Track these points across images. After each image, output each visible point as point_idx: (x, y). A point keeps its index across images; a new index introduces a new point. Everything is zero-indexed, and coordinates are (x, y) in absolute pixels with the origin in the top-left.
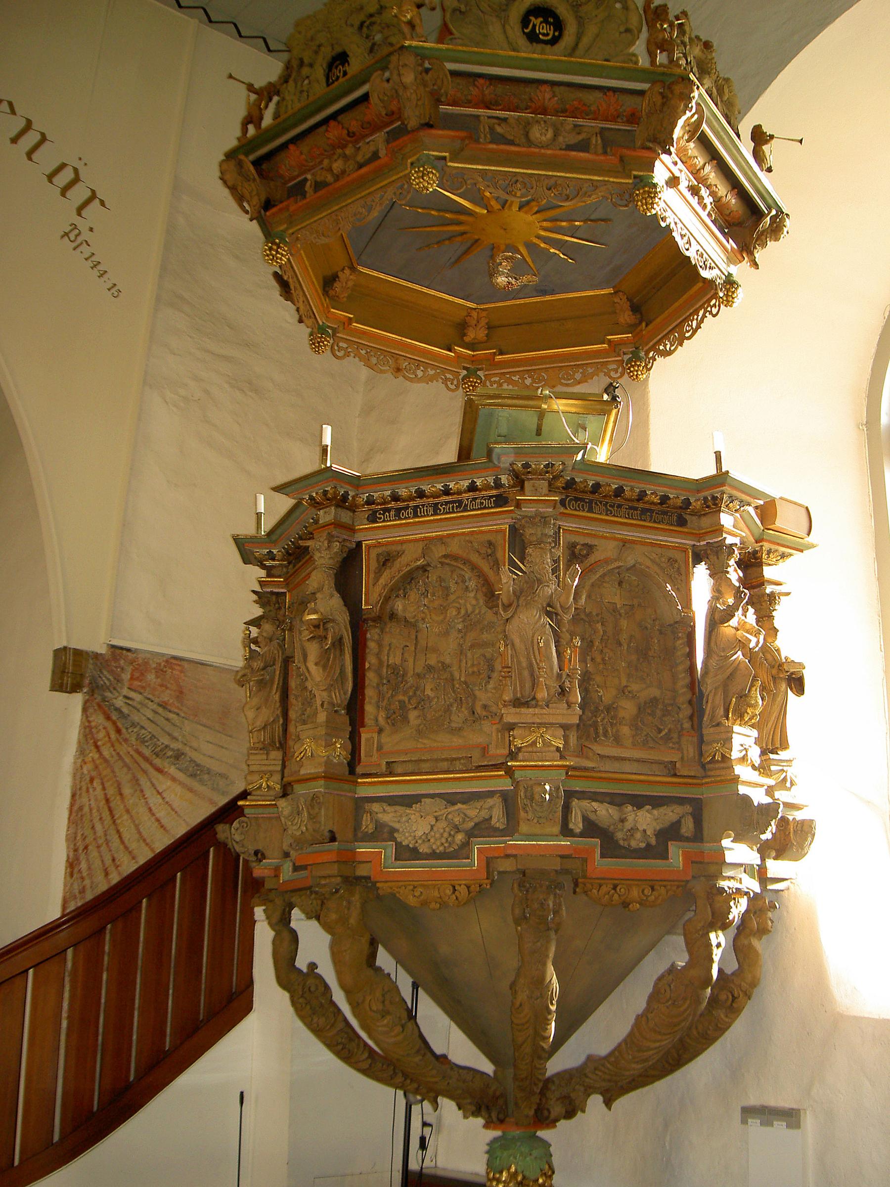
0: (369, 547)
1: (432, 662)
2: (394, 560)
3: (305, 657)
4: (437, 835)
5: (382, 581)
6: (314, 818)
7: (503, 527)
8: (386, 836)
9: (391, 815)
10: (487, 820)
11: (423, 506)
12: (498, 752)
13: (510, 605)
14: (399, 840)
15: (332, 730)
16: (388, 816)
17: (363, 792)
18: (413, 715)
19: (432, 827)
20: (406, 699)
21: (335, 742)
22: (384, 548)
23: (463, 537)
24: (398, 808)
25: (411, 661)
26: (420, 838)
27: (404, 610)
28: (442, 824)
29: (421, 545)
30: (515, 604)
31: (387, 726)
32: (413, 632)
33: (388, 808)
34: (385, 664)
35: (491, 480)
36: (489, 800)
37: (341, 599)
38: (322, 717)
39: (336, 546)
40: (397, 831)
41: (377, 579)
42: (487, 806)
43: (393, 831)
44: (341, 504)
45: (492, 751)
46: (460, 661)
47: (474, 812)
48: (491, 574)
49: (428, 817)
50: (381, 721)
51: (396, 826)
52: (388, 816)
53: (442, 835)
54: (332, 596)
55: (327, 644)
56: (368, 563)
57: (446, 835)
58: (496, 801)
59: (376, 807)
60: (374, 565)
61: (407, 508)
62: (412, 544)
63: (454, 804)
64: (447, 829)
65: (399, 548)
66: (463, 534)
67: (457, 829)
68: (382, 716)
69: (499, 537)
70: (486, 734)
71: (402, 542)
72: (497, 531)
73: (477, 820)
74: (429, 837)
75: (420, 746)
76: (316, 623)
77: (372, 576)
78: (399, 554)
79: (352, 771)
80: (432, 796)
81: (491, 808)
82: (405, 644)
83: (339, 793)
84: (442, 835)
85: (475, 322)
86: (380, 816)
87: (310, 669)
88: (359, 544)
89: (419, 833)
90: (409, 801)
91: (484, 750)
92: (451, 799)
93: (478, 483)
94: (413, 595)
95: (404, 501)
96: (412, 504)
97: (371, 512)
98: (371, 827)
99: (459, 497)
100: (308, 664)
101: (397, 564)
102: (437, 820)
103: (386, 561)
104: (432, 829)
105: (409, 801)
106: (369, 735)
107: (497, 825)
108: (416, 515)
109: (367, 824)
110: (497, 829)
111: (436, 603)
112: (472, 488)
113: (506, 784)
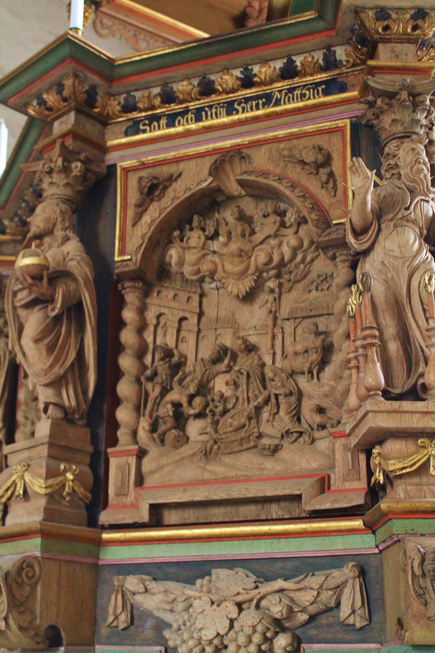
0: (126, 171)
1: (228, 340)
2: (165, 188)
3: (20, 330)
4: (242, 639)
5: (147, 218)
6: (22, 604)
7: (340, 123)
8: (149, 633)
9: (159, 598)
10: (331, 609)
11: (211, 107)
12: (347, 485)
13: (365, 230)
14: (171, 643)
15: (59, 450)
16: (154, 599)
17: (112, 555)
18: (194, 428)
19: (232, 621)
20: (184, 401)
21: (65, 471)
22: (150, 170)
23: (276, 145)
24: (171, 585)
25: (191, 339)
26: (210, 642)
27: (181, 263)
28: (249, 617)
29: (208, 161)
30: (374, 227)
31: (152, 444)
32: (196, 299)
33: (153, 585)
34: (151, 346)
35: (319, 56)
36: (335, 573)
37: (79, 244)
38: (44, 428)
39: (77, 167)
40: (169, 626)
41: (139, 217)
42: (332, 583)
43: (161, 626)
44: (85, 109)
45: (336, 482)
46: (274, 337)
47: (307, 594)
48: (324, 198)
49: (224, 604)
50: (143, 435)
51: (168, 617)
52: (154, 599)
53: (250, 640)
54: (66, 239)
55: (53, 310)
56: (126, 193)
57: (257, 638)
58: (348, 571)
59: (132, 583)
60: (134, 197)
61: (186, 112)
62: (194, 161)
63: (268, 579)
64: (260, 628)
65: (173, 169)
66: (277, 140)
67: (279, 625)
68: (144, 424)
69: (336, 139)
70: (333, 454)
71: (177, 160)
72: (330, 131)
73: (312, 609)
74: (226, 642)
75: (206, 476)
76: (35, 271)
77: (131, 213)
78: (171, 179)
79: (92, 522)
80: (230, 563)
81: (339, 589)
82: (182, 314)
83: (69, 558)
84: (250, 640)
85: (256, 14)
86: (138, 598)
87: (26, 350)
88: (113, 167)
89: (209, 634)
90: (193, 571)
91: (324, 485)
92: (263, 569)
93: (298, 60)
94: (195, 238)
95: (181, 102)
96: (193, 105)
97: (130, 123)
98: (122, 618)
99: (267, 89)
100: (23, 342)
101: (170, 193)
102: (241, 610)
103: (153, 190)
104: (231, 626)
105: (193, 571)
106: (122, 460)
107: (351, 621)
108: (198, 119)
109: (114, 613)
110: (347, 627)
111: (234, 247)
112: (289, 72)
113: (366, 543)
